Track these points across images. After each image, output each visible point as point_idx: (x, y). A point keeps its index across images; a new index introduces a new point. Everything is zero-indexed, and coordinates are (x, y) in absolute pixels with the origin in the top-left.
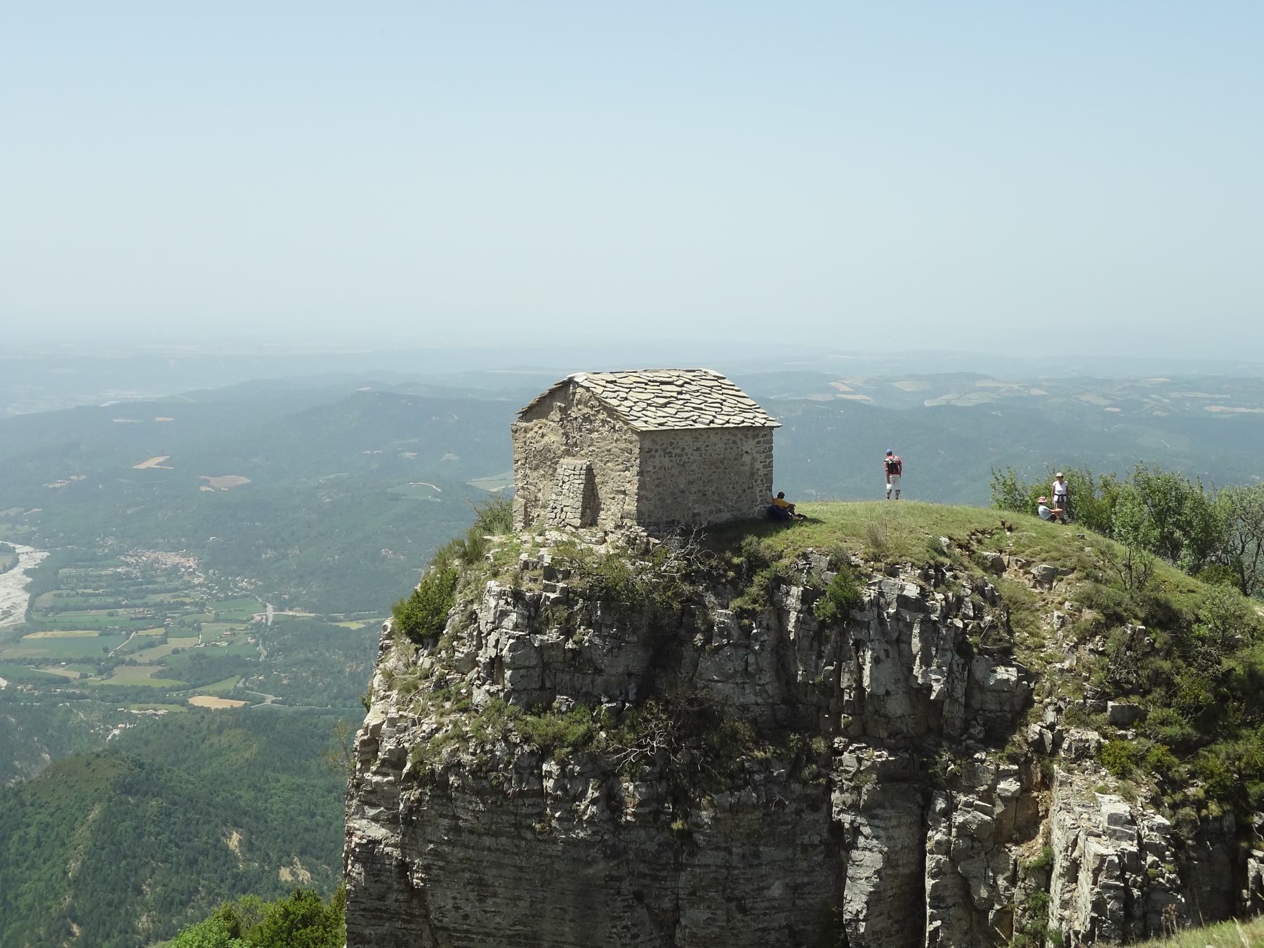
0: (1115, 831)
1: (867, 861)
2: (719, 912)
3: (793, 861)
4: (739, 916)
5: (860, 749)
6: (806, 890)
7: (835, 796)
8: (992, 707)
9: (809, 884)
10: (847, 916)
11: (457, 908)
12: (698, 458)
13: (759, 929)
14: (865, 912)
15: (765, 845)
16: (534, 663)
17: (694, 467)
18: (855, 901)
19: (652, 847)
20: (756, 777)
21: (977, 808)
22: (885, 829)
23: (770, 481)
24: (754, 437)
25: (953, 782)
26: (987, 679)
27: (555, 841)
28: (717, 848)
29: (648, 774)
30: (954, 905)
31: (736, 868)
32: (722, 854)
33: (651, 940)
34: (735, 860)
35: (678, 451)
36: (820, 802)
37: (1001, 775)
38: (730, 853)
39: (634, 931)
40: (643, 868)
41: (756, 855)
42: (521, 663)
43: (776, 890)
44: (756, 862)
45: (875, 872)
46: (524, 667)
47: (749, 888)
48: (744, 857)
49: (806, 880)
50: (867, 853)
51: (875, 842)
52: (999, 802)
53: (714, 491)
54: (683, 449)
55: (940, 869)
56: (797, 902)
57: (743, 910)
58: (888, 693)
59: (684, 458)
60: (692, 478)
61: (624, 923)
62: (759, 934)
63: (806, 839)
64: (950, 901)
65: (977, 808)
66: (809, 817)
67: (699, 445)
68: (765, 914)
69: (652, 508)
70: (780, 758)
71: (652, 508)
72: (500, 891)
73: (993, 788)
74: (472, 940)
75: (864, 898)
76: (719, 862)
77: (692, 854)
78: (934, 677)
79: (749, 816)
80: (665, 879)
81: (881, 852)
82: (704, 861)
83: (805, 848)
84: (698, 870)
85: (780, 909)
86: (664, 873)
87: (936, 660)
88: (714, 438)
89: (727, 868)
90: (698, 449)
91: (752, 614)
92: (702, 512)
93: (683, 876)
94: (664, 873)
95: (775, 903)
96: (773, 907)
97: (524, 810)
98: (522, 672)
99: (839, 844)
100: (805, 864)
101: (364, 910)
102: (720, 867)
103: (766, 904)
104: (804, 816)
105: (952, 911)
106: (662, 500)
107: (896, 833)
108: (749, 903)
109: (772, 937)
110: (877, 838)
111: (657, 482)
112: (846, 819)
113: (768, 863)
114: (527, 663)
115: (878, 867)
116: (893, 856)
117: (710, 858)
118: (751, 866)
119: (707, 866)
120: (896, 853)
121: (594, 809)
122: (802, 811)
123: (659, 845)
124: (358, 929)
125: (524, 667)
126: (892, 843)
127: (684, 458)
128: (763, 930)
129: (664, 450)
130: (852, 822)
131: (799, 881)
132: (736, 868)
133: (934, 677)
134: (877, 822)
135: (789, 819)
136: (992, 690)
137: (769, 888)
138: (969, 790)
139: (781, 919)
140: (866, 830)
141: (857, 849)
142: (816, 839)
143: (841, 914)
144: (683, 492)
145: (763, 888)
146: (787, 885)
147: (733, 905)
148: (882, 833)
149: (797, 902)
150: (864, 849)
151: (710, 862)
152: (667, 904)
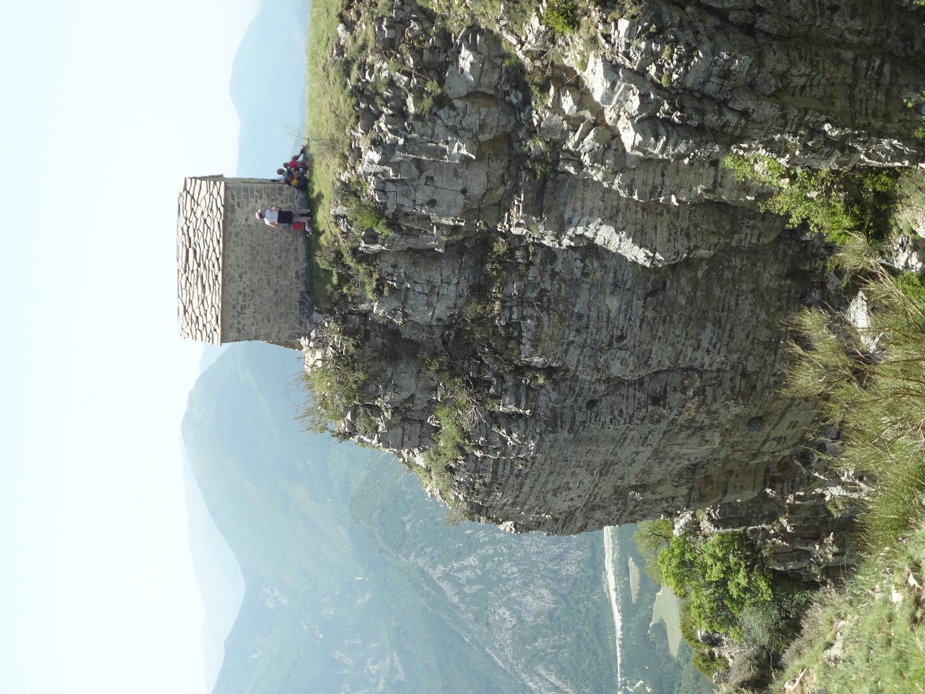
0: (618, 101)
1: (605, 235)
2: (618, 355)
3: (593, 285)
4: (625, 342)
5: (509, 220)
6: (620, 278)
7: (547, 242)
8: (496, 76)
9: (615, 273)
10: (648, 265)
11: (572, 499)
12: (248, 276)
13: (641, 327)
14: (648, 251)
15: (574, 307)
16: (400, 430)
17: (255, 280)
18: (636, 254)
19: (554, 395)
20: (514, 316)
21: (581, 139)
22: (582, 216)
23: (273, 181)
24: (233, 211)
25: (555, 146)
26: (468, 81)
27: (534, 458)
28: (566, 352)
29: (497, 391)
30: (663, 175)
31: (585, 341)
32: (572, 349)
33: (627, 398)
34: (579, 340)
35: (241, 298)
36: (550, 254)
37: (557, 107)
38: (573, 342)
39: (616, 413)
40: (569, 402)
41: (580, 317)
42: (399, 440)
43: (613, 303)
44: (585, 319)
45: (617, 233)
46: (403, 437)
47: (604, 332)
48: (578, 331)
49: (612, 275)
50: (599, 233)
51: (591, 226)
52: (582, 113)
53: (279, 261)
54: (240, 293)
55: (627, 186)
56: (627, 287)
57: (621, 338)
58: (464, 191)
59: (248, 291)
60: (265, 282)
61: (608, 421)
62: (644, 325)
63: (578, 273)
64: (658, 181)
65: (581, 139)
66: (558, 267)
67: (236, 275)
68: (630, 319)
69: (287, 326)
70: (504, 284)
71: (287, 326)
72: (565, 481)
73: (567, 118)
74: (598, 493)
75: (636, 248)
76: (577, 352)
77: (567, 370)
78: (455, 151)
79: (546, 327)
80: (581, 389)
81: (601, 224)
82: (574, 363)
83: (584, 274)
84: (580, 368)
85: (629, 304)
86: (577, 389)
87: (441, 145)
88: (232, 260)
89: (584, 347)
90: (241, 277)
91: (381, 282)
92: (295, 269)
93: (582, 377)
94: (577, 389)
95: (624, 307)
96: (626, 311)
97: (507, 472)
98: (406, 439)
99: (590, 250)
100: (598, 274)
101: (563, 527)
102: (582, 351)
103: (622, 316)
104: (557, 270)
105: (667, 183)
106: (281, 315)
107: (589, 204)
108: (617, 333)
109: (650, 314)
110: (588, 224)
111: (266, 321)
112: (566, 242)
113: (589, 307)
114: (400, 436)
115: (613, 230)
116: (607, 214)
117: (572, 359)
118: (587, 327)
119: (578, 361)
120: (605, 208)
121: (515, 435)
122: (553, 270)
123: (554, 390)
124: (576, 530)
125: (403, 437)
126: (596, 213)
127: (248, 291)
128: (642, 321)
129: (239, 314)
130: (571, 239)
131: (611, 280)
132: (585, 341)
133: (455, 151)
134: (575, 221)
135: (557, 286)
136: (478, 80)
137: (609, 311)
138: (565, 135)
139: (638, 304)
140: (580, 230)
141: (594, 238)
142: (579, 264)
143: (644, 267)
144: (276, 292)
145: (608, 318)
146: (612, 293)
147: (615, 344)
148: (585, 219)
149: (627, 287)
150: (596, 234)
151: (576, 358)
152: (602, 388)
